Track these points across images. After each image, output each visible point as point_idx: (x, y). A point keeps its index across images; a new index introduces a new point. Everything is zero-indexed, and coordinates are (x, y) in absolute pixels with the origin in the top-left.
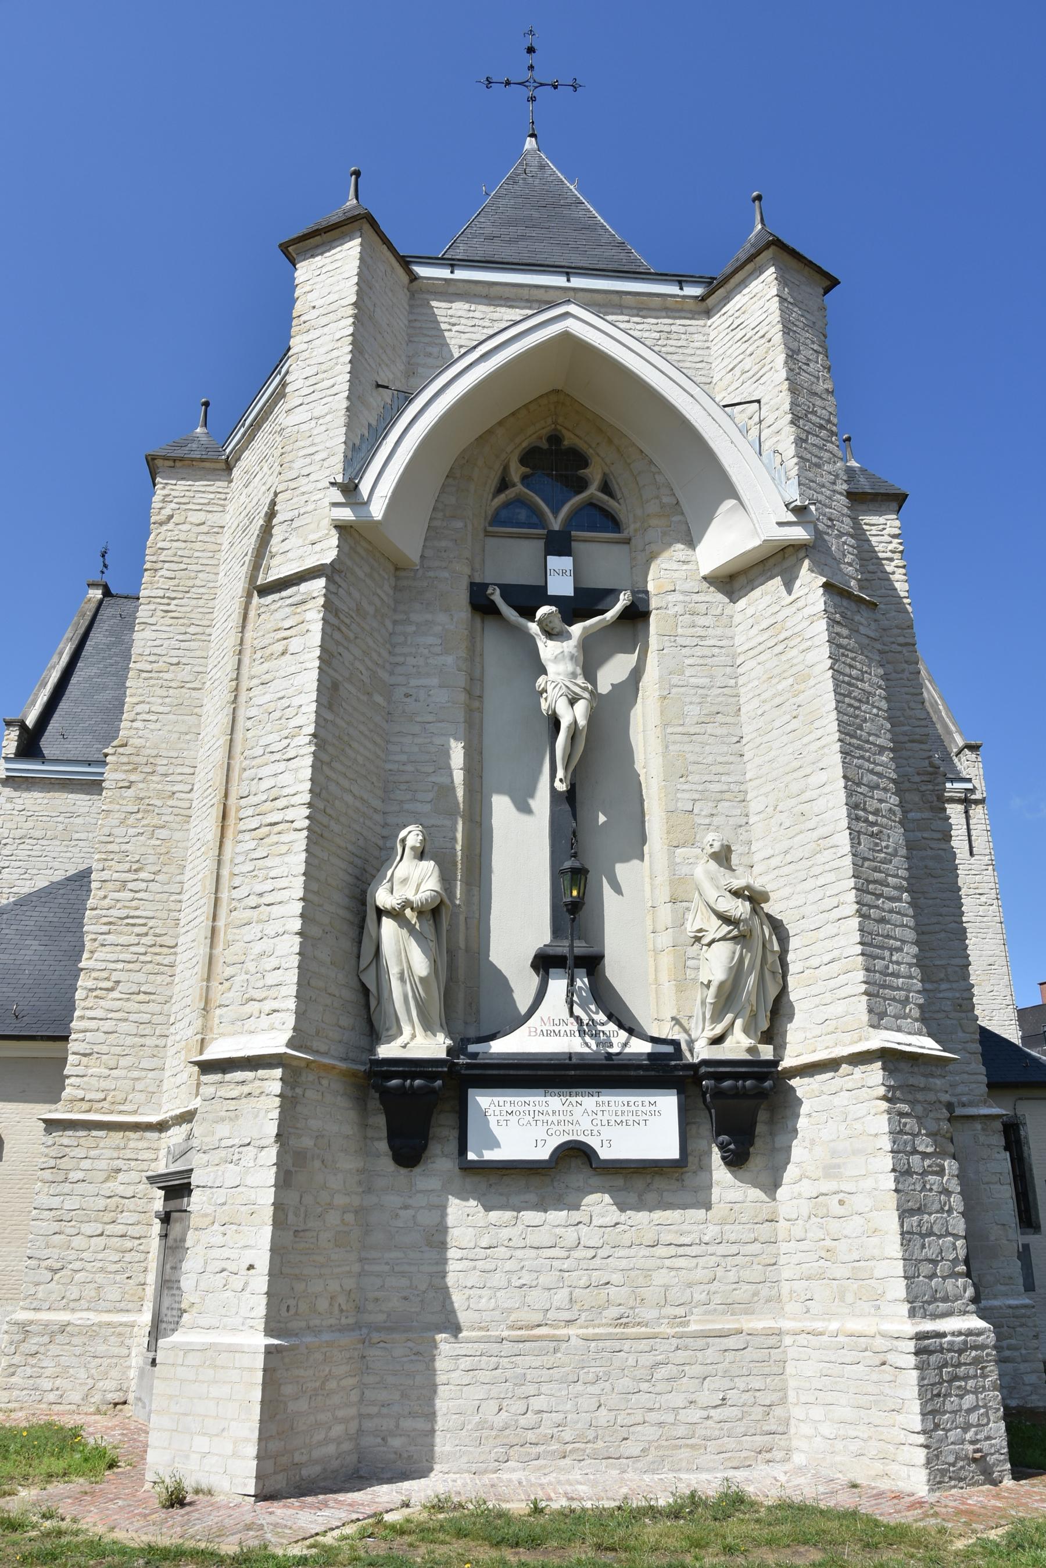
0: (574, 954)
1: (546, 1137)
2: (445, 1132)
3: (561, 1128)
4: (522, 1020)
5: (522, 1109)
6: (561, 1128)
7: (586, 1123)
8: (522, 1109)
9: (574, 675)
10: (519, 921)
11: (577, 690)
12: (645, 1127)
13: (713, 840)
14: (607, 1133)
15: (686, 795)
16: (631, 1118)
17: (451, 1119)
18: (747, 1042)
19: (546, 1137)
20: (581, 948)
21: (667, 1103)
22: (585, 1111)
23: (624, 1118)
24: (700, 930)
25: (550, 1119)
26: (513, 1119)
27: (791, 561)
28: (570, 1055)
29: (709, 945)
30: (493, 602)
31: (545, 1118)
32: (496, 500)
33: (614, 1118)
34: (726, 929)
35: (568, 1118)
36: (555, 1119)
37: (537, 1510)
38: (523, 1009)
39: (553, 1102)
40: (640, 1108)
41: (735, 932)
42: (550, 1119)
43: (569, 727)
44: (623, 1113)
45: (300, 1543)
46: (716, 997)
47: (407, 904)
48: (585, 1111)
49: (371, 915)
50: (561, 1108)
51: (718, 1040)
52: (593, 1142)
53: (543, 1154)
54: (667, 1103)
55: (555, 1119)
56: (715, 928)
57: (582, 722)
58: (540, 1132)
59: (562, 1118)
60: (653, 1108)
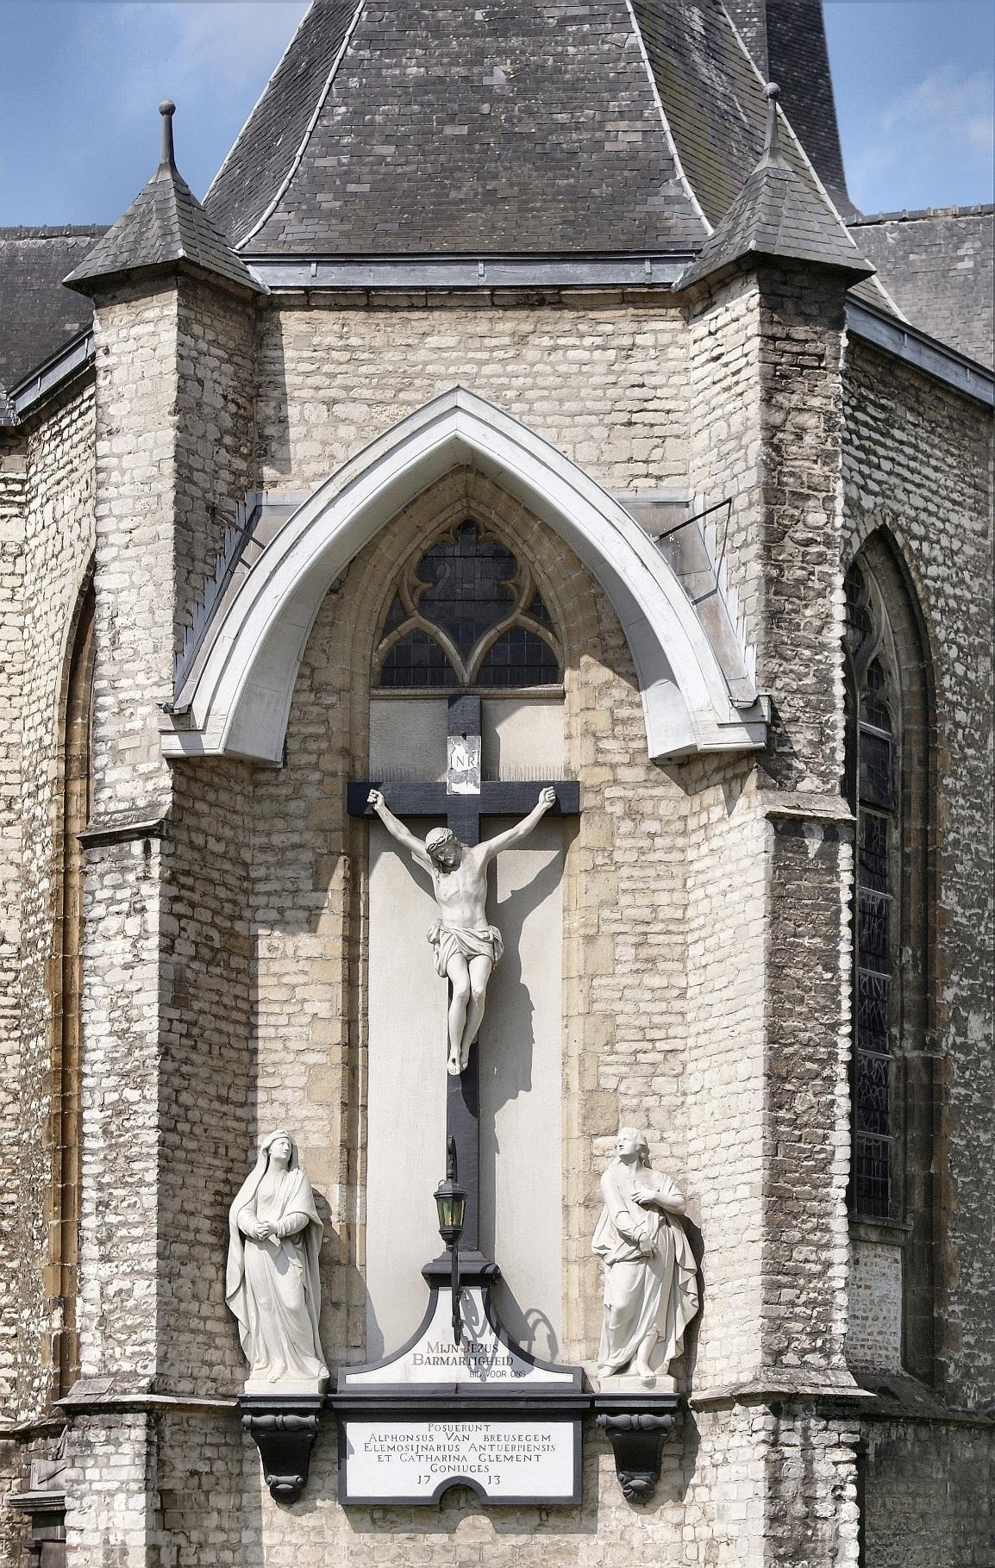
0: (468, 1269)
1: (430, 1473)
2: (327, 1467)
3: (446, 1464)
4: (389, 1361)
5: (404, 1444)
6: (446, 1464)
7: (472, 1458)
8: (404, 1444)
9: (472, 921)
10: (399, 1229)
11: (474, 944)
12: (541, 1460)
13: (628, 1138)
14: (495, 1468)
15: (612, 1070)
16: (522, 1453)
17: (333, 1454)
18: (646, 1373)
19: (430, 1473)
20: (470, 1262)
21: (563, 1434)
22: (473, 1446)
23: (514, 1454)
24: (603, 1247)
25: (435, 1454)
26: (395, 1455)
27: (740, 769)
28: (457, 1386)
29: (611, 1264)
30: (376, 812)
31: (429, 1453)
32: (385, 641)
33: (503, 1453)
34: (628, 1248)
35: (453, 1453)
36: (440, 1454)
37: (81, 1279)
38: (387, 1353)
39: (438, 1432)
40: (533, 1442)
41: (636, 1253)
42: (435, 1454)
43: (462, 997)
44: (513, 1448)
45: (449, 481)
46: (618, 1322)
47: (271, 1230)
48: (473, 1446)
49: (234, 1239)
50: (447, 1443)
51: (622, 1369)
52: (480, 1478)
53: (427, 1490)
54: (563, 1434)
55: (440, 1454)
56: (618, 1249)
57: (479, 988)
58: (424, 1467)
59: (447, 1453)
60: (546, 1442)
